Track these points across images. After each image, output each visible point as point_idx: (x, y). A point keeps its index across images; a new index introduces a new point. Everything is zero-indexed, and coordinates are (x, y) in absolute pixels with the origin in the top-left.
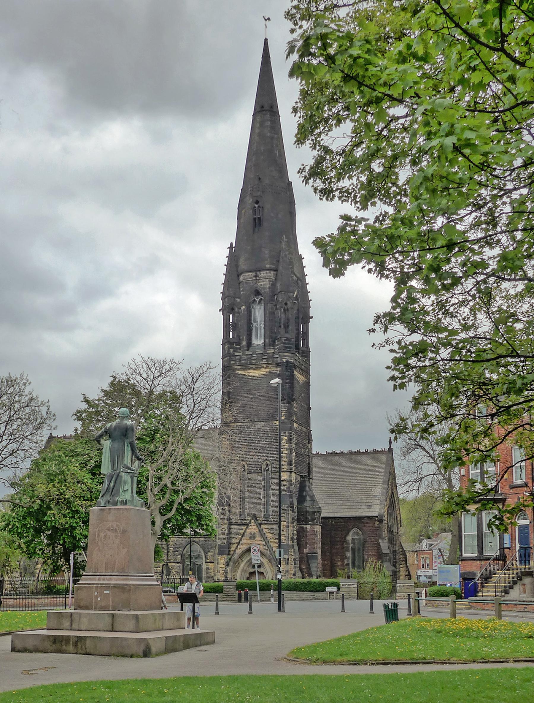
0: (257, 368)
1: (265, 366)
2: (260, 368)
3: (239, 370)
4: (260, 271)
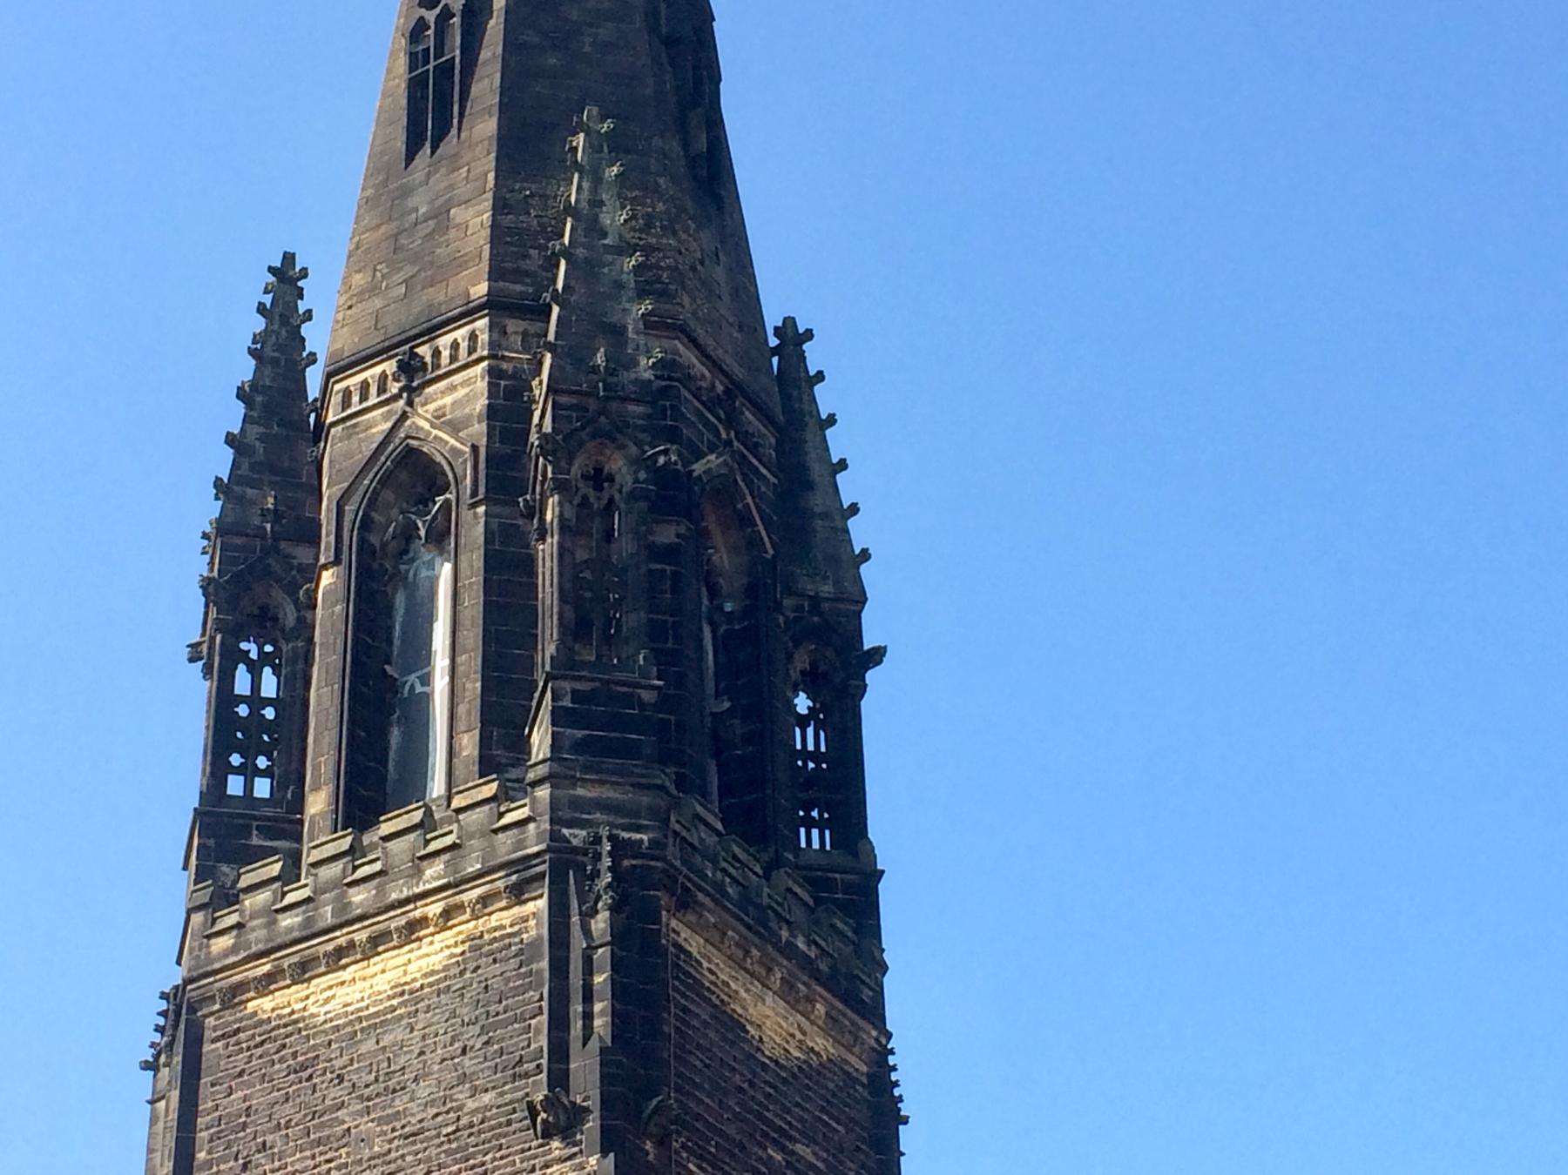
0: (377, 943)
1: (434, 909)
2: (412, 930)
3: (265, 984)
4: (431, 331)
